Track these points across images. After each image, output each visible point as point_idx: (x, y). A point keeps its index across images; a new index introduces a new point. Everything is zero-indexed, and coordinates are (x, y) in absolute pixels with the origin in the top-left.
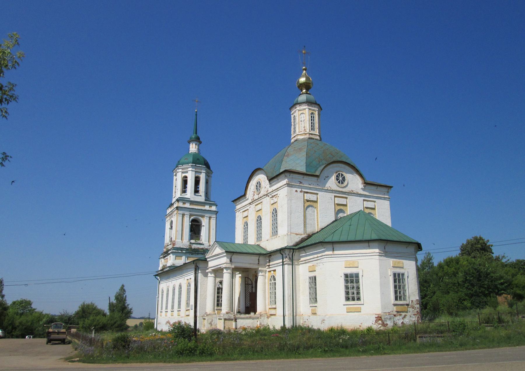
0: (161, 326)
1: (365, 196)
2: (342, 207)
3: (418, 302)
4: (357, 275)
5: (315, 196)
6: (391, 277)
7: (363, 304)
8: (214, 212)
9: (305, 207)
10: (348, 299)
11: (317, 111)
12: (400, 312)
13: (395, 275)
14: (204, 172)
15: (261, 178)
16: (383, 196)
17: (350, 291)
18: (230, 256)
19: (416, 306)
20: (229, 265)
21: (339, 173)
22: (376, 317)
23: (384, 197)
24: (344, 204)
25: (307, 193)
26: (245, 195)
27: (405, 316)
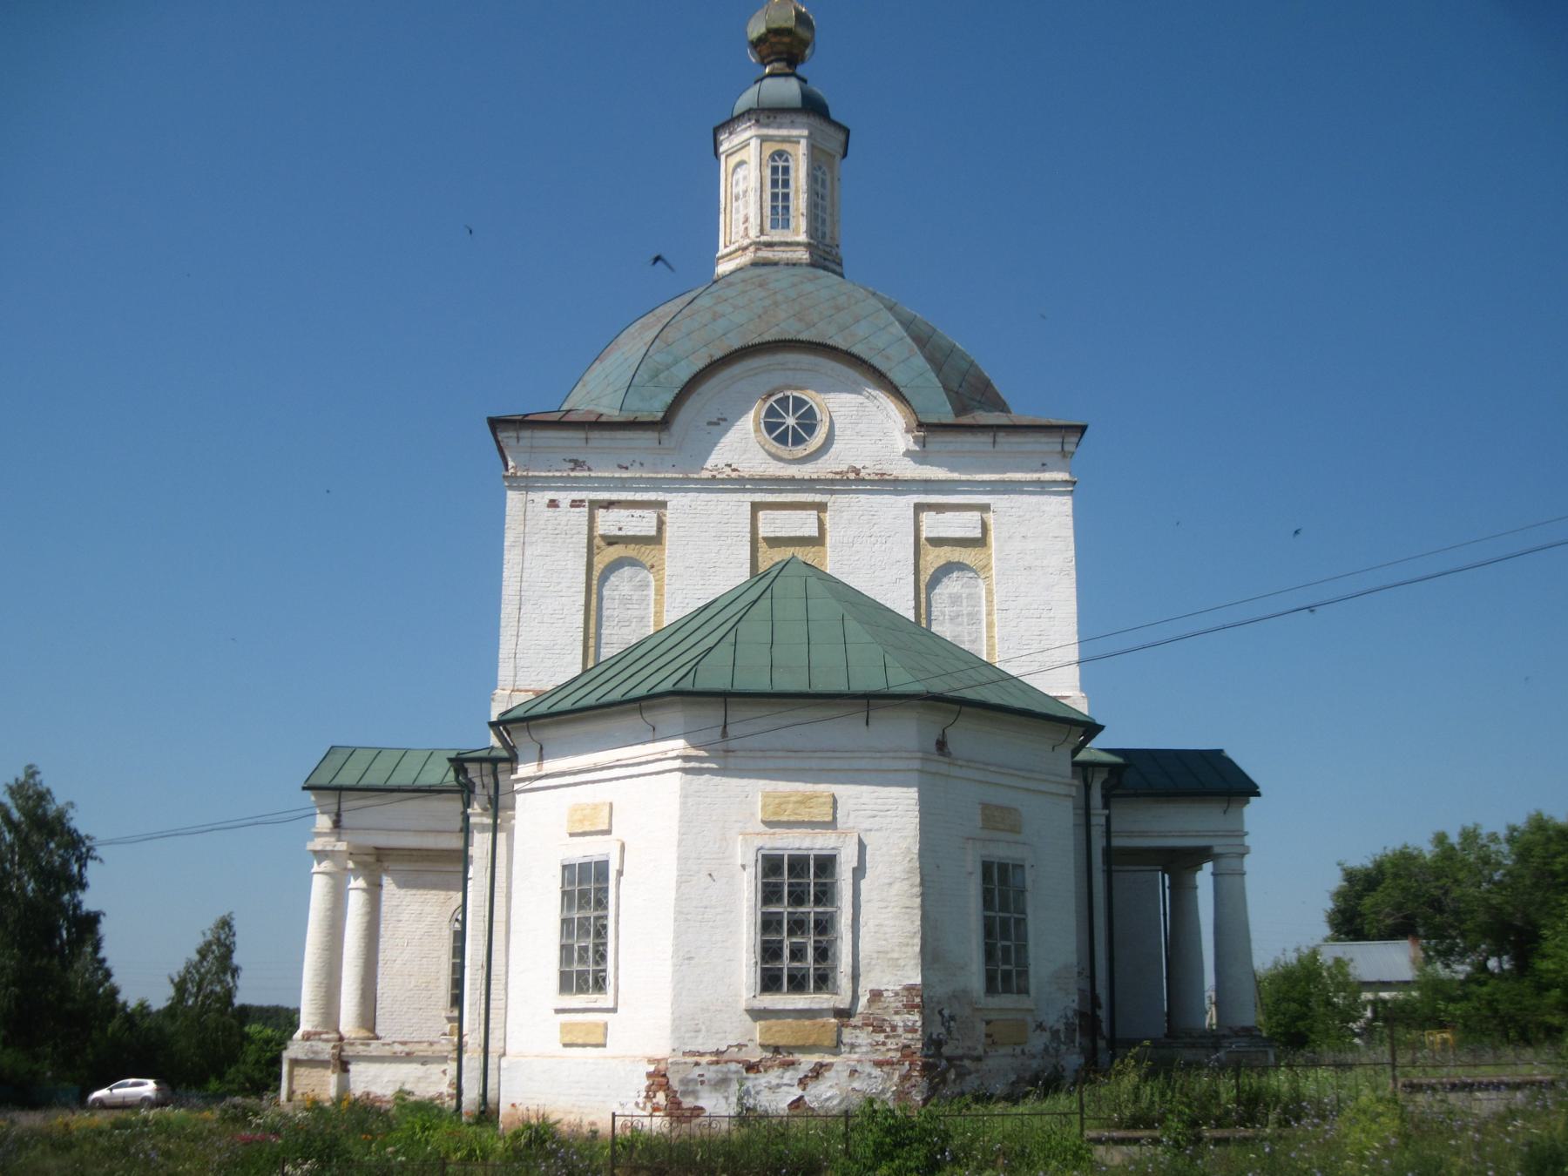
1: (928, 486)
3: (918, 1000)
4: (826, 864)
6: (745, 874)
7: (614, 1010)
9: (598, 568)
11: (803, 142)
12: (791, 1050)
13: (987, 868)
16: (1035, 476)
18: (330, 801)
19: (898, 1020)
20: (327, 839)
21: (781, 395)
22: (649, 1075)
23: (1039, 482)
24: (806, 534)
25: (609, 505)
27: (818, 1072)
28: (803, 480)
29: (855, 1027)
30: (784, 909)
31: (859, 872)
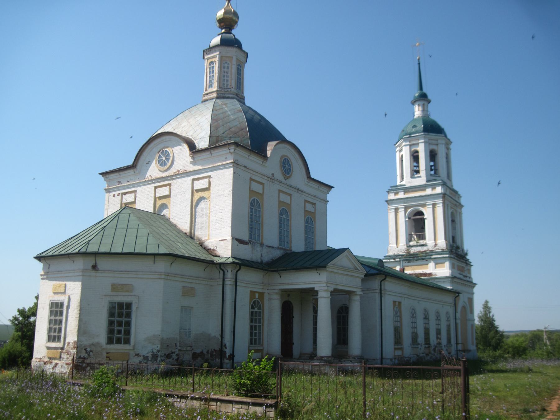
0: (125, 362)
2: (163, 200)
3: (76, 345)
5: (133, 195)
8: (437, 196)
14: (422, 142)
24: (166, 194)
28: (165, 177)
29: (64, 353)
30: (124, 319)
31: (68, 307)
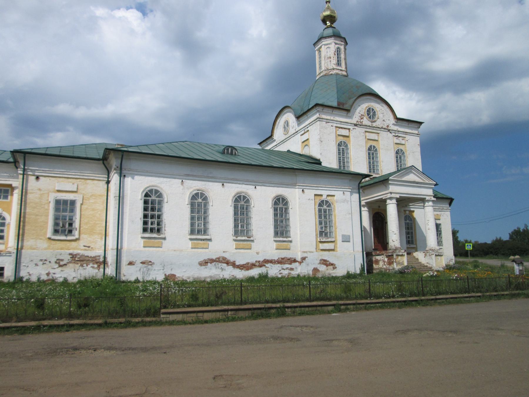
10: (145, 230)
15: (289, 117)
17: (156, 225)
25: (340, 128)
26: (271, 136)
